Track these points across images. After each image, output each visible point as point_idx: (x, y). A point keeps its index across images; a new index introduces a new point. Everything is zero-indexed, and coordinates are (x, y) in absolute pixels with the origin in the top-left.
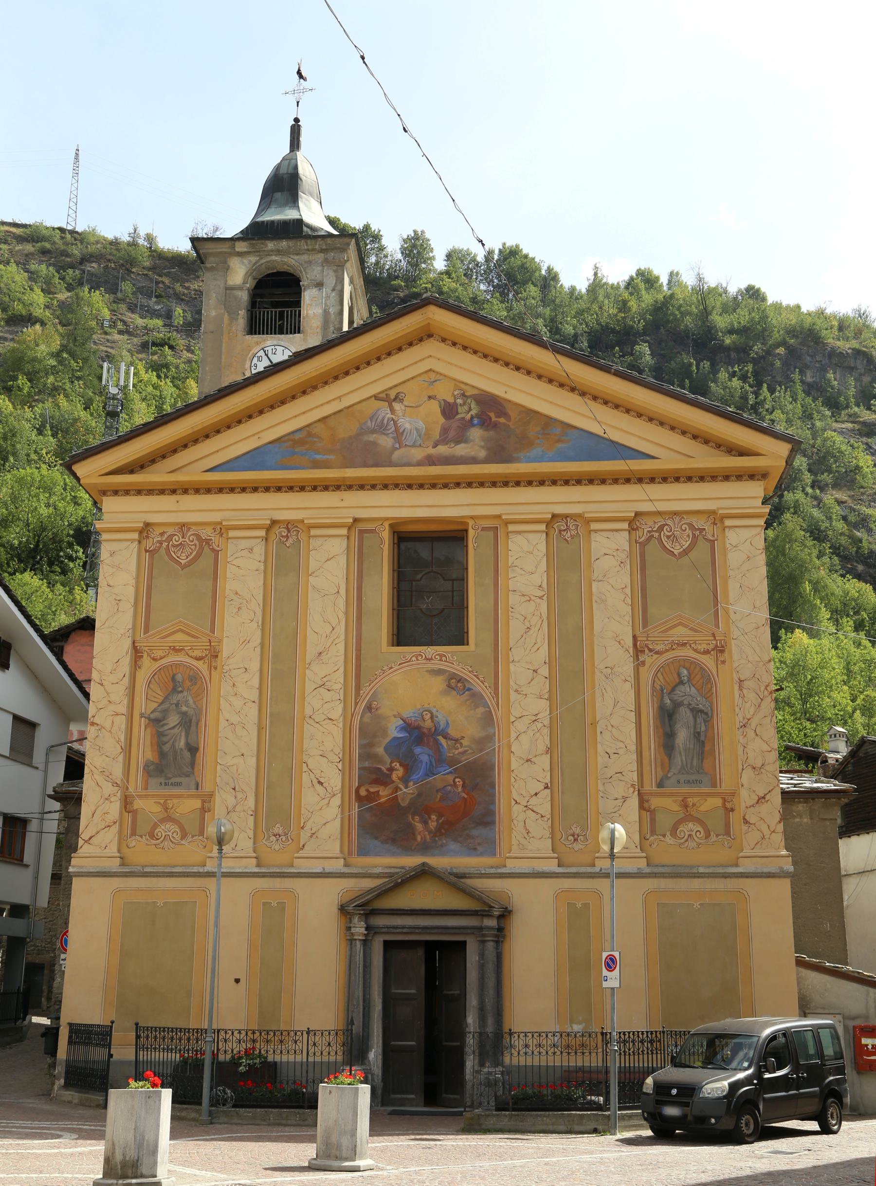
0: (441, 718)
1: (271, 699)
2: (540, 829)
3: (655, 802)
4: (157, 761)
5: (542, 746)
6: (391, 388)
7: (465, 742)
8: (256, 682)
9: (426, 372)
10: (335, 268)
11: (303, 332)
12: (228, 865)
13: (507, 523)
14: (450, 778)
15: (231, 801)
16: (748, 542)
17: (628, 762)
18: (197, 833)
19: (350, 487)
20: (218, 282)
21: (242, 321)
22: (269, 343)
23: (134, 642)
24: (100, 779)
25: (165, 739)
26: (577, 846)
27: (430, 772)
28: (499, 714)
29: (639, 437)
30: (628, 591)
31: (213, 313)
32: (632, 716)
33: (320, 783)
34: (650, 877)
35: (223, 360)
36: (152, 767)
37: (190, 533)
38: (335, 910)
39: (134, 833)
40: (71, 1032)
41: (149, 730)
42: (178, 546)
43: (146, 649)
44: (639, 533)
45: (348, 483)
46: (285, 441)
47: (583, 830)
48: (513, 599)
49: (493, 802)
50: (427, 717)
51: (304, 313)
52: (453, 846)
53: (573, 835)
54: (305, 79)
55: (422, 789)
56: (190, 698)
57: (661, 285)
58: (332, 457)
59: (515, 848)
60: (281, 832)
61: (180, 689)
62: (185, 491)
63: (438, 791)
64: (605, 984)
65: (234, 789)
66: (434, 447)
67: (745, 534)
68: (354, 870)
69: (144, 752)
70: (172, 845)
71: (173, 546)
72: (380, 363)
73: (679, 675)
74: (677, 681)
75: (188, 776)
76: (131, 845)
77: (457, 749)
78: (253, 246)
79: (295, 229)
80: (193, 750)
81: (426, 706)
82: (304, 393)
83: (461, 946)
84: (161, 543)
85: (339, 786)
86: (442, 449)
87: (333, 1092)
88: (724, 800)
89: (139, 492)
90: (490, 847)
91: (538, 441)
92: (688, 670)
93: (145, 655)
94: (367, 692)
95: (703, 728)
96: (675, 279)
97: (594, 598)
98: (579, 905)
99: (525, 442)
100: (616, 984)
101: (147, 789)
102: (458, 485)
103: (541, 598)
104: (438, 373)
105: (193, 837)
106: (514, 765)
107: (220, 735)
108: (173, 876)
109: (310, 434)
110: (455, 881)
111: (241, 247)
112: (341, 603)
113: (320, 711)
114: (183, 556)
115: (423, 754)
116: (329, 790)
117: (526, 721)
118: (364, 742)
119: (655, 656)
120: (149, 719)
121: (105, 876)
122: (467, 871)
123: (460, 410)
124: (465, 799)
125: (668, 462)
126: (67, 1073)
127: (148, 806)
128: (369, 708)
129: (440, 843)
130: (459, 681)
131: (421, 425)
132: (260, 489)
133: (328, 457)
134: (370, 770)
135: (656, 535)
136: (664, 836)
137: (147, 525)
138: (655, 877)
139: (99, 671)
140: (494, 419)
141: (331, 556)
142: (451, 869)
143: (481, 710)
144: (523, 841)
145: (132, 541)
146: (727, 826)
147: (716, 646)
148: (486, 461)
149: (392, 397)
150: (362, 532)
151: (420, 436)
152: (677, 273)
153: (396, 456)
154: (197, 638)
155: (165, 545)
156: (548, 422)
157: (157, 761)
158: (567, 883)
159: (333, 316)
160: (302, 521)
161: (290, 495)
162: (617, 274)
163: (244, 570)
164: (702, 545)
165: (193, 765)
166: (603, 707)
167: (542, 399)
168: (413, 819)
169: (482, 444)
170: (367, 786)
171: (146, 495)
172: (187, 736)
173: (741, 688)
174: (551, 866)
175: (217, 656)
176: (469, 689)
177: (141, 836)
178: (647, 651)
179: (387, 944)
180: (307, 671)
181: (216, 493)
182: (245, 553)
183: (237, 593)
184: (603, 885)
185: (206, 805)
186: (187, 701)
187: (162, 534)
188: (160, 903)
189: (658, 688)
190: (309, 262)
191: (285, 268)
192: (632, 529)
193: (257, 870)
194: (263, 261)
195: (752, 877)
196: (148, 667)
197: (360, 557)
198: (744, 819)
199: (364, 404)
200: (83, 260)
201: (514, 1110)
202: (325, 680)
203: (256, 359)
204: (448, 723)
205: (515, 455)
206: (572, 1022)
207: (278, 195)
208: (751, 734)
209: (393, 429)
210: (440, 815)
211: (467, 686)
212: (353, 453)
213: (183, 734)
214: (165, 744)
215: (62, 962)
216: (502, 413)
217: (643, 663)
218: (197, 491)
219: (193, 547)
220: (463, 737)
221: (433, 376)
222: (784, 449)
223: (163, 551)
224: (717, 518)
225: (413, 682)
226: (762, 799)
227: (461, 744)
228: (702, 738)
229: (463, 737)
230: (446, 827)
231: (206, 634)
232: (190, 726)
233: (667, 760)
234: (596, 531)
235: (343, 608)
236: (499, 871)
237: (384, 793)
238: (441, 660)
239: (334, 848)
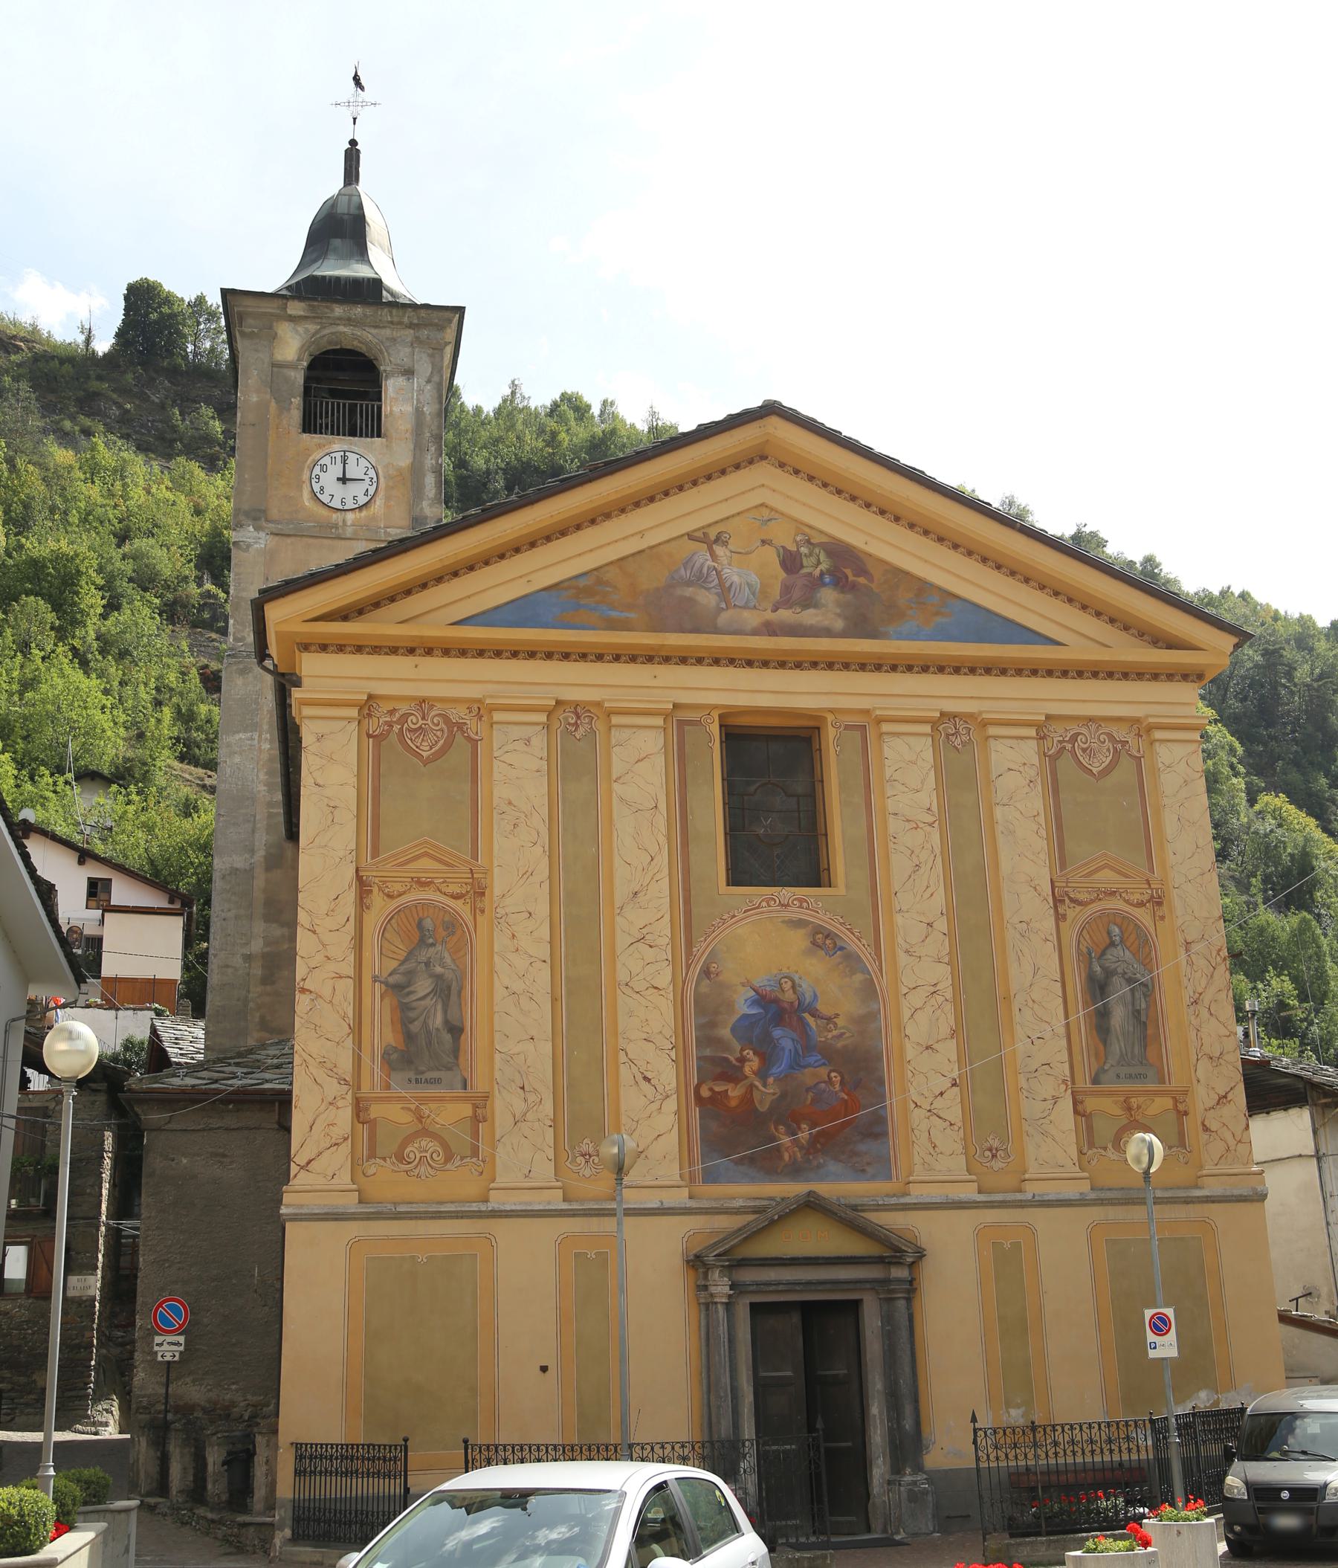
0: (805, 986)
1: (566, 956)
2: (950, 1142)
3: (1090, 1104)
4: (402, 1046)
5: (945, 1030)
6: (709, 525)
7: (840, 1022)
8: (545, 932)
10: (430, 351)
11: (386, 436)
12: (632, 1198)
13: (879, 721)
14: (823, 1072)
15: (519, 1106)
16: (1184, 761)
17: (1055, 1050)
18: (469, 1153)
19: (667, 660)
21: (296, 415)
22: (336, 447)
23: (357, 870)
24: (321, 1075)
25: (412, 1014)
26: (997, 1165)
27: (796, 1064)
28: (883, 983)
29: (1041, 615)
30: (1042, 819)
31: (254, 398)
33: (646, 1079)
34: (1095, 1205)
35: (269, 467)
36: (395, 1056)
37: (433, 713)
38: (678, 1262)
40: (300, 1458)
41: (387, 1001)
42: (416, 730)
43: (377, 880)
44: (1048, 743)
45: (664, 654)
48: (894, 825)
50: (787, 986)
51: (386, 409)
52: (833, 1167)
53: (990, 1150)
54: (362, 88)
55: (784, 1089)
56: (446, 955)
57: (593, 417)
58: (632, 615)
59: (918, 1168)
60: (591, 1150)
61: (431, 941)
62: (429, 652)
63: (808, 1090)
64: (1152, 1354)
65: (523, 1088)
66: (774, 611)
67: (1180, 751)
68: (705, 1204)
69: (382, 1033)
71: (410, 730)
73: (1109, 933)
74: (1108, 941)
75: (449, 1069)
76: (371, 1171)
77: (830, 1031)
78: (312, 308)
79: (371, 291)
80: (456, 1030)
81: (785, 970)
82: (593, 522)
83: (855, 1305)
84: (390, 725)
85: (674, 1084)
86: (785, 615)
87: (1185, 1532)
88: (1176, 1101)
89: (359, 649)
90: (882, 1166)
92: (1120, 928)
93: (375, 889)
94: (702, 950)
95: (1143, 1006)
96: (609, 410)
97: (999, 828)
98: (1007, 1245)
100: (1173, 1353)
103: (931, 825)
104: (772, 509)
105: (462, 1159)
106: (910, 1053)
107: (496, 1009)
108: (440, 1218)
109: (600, 582)
110: (847, 1218)
111: (296, 308)
112: (661, 822)
113: (641, 977)
114: (425, 746)
115: (785, 1039)
116: (660, 1089)
119: (1078, 908)
120: (387, 984)
121: (336, 1220)
122: (859, 1202)
123: (805, 563)
125: (1077, 651)
126: (297, 1520)
127: (393, 1114)
128: (706, 972)
129: (815, 1163)
130: (827, 937)
131: (754, 579)
132: (539, 655)
133: (627, 615)
134: (712, 1060)
135: (1069, 746)
136: (1105, 1149)
137: (370, 697)
139: (309, 912)
140: (851, 578)
141: (643, 755)
142: (838, 1199)
144: (928, 1159)
145: (350, 720)
146: (1181, 1134)
147: (1152, 897)
148: (844, 634)
149: (713, 537)
150: (682, 723)
151: (754, 594)
152: (612, 404)
153: (723, 619)
154: (452, 866)
155: (396, 728)
156: (923, 587)
157: (402, 1046)
159: (428, 418)
160: (598, 704)
161: (531, 664)
162: (540, 397)
163: (518, 772)
164: (1126, 762)
165: (456, 1052)
167: (915, 556)
168: (776, 1129)
169: (838, 611)
170: (710, 1084)
171: (369, 653)
172: (445, 1011)
173: (1187, 950)
174: (969, 1192)
175: (483, 894)
176: (841, 948)
177: (384, 1159)
178: (1067, 901)
179: (755, 1308)
180: (618, 919)
181: (473, 657)
182: (520, 746)
183: (510, 803)
184: (1038, 1217)
185: (479, 1111)
186: (442, 959)
187: (392, 712)
188: (422, 1258)
189: (1085, 950)
191: (355, 345)
192: (1041, 738)
193: (565, 1206)
194: (326, 331)
195: (1219, 1202)
196: (380, 908)
197: (681, 759)
198: (1204, 1125)
201: (1049, 1534)
202: (644, 931)
204: (815, 996)
206: (1008, 1405)
207: (337, 242)
208: (1204, 1013)
209: (716, 582)
211: (839, 943)
213: (439, 1007)
214: (412, 1021)
215: (156, 1348)
216: (862, 571)
217: (1064, 917)
218: (446, 652)
219: (439, 733)
222: (1228, 641)
223: (393, 737)
224: (1142, 728)
225: (764, 937)
226: (1223, 1098)
227: (835, 1024)
228: (1143, 1018)
230: (822, 1140)
231: (467, 862)
232: (449, 996)
233: (1101, 1047)
234: (996, 738)
235: (664, 831)
236: (903, 1200)
237: (735, 1092)
238: (801, 907)
239: (672, 1172)
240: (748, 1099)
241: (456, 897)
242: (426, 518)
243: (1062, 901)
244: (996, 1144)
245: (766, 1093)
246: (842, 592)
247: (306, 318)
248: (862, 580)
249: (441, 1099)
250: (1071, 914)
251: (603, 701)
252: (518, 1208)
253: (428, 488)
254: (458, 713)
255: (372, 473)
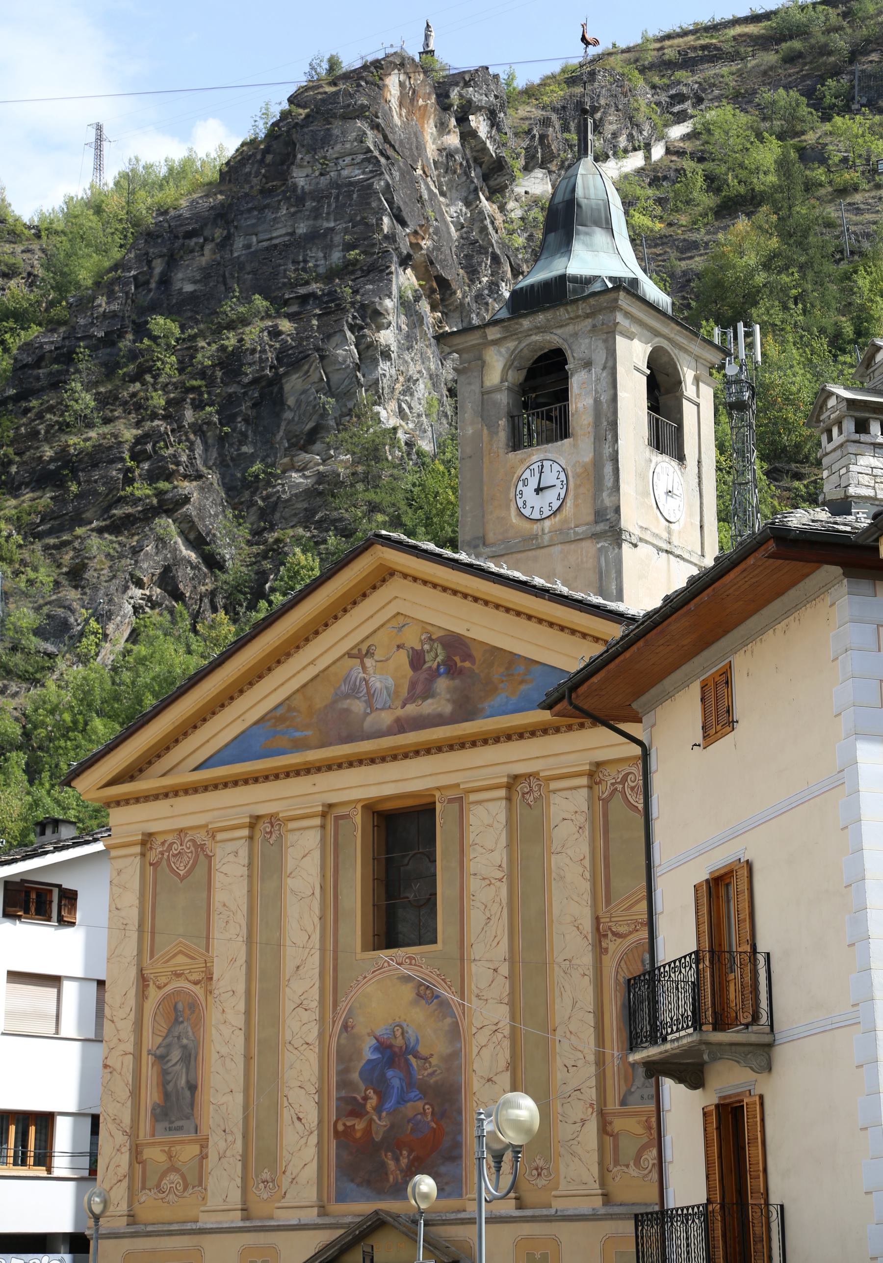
0: (411, 1033)
4: (162, 1104)
6: (362, 641)
7: (434, 1061)
8: (242, 1007)
9: (394, 616)
10: (604, 336)
14: (420, 1104)
19: (319, 770)
20: (473, 387)
21: (503, 435)
22: (535, 458)
25: (169, 1078)
26: (541, 1182)
27: (402, 1100)
31: (470, 431)
32: (590, 1019)
33: (299, 1119)
34: (606, 1219)
36: (158, 1111)
39: (143, 1188)
44: (602, 787)
46: (269, 720)
47: (546, 1162)
49: (460, 1132)
50: (398, 1033)
51: (572, 407)
53: (537, 1169)
56: (189, 1029)
58: (309, 733)
63: (409, 1121)
66: (403, 707)
69: (150, 1096)
70: (176, 1199)
71: (174, 856)
72: (348, 615)
75: (188, 1118)
76: (142, 1200)
80: (193, 1088)
81: (397, 1020)
86: (411, 709)
91: (501, 686)
93: (151, 983)
98: (538, 1256)
99: (491, 689)
101: (153, 1135)
102: (417, 753)
103: (500, 880)
106: (476, 1085)
109: (290, 709)
115: (394, 1076)
117: (487, 1031)
118: (341, 1067)
120: (155, 1055)
123: (427, 659)
124: (434, 1130)
127: (155, 1155)
128: (345, 1027)
131: (391, 682)
136: (627, 1166)
138: (612, 1219)
139: (110, 1007)
140: (459, 664)
143: (449, 1020)
145: (135, 855)
149: (364, 652)
150: (337, 818)
156: (512, 659)
157: (162, 1104)
158: (527, 1229)
165: (192, 1105)
166: (561, 1008)
169: (448, 696)
178: (610, 935)
182: (231, 858)
184: (564, 1230)
187: (163, 843)
190: (575, 335)
193: (241, 1224)
196: (154, 995)
199: (338, 664)
200: (854, 55)
203: (521, 483)
204: (417, 1040)
205: (480, 706)
210: (411, 1151)
212: (326, 728)
214: (168, 1083)
216: (468, 656)
217: (606, 950)
220: (432, 1055)
221: (400, 621)
223: (164, 863)
225: (386, 991)
229: (432, 1055)
235: (317, 911)
237: (360, 1125)
239: (310, 1194)
240: (368, 1131)
241: (196, 983)
242: (606, 508)
243: (606, 936)
244: (541, 1163)
245: (381, 1124)
246: (453, 679)
247: (505, 338)
248: (467, 664)
249: (182, 1142)
250: (612, 947)
251: (277, 813)
252: (214, 1226)
253: (607, 478)
254: (201, 837)
255: (563, 476)
